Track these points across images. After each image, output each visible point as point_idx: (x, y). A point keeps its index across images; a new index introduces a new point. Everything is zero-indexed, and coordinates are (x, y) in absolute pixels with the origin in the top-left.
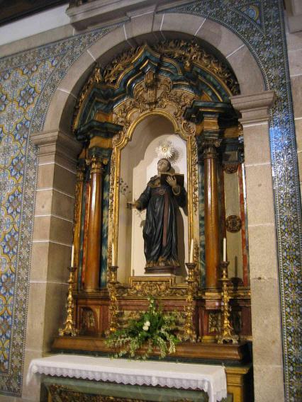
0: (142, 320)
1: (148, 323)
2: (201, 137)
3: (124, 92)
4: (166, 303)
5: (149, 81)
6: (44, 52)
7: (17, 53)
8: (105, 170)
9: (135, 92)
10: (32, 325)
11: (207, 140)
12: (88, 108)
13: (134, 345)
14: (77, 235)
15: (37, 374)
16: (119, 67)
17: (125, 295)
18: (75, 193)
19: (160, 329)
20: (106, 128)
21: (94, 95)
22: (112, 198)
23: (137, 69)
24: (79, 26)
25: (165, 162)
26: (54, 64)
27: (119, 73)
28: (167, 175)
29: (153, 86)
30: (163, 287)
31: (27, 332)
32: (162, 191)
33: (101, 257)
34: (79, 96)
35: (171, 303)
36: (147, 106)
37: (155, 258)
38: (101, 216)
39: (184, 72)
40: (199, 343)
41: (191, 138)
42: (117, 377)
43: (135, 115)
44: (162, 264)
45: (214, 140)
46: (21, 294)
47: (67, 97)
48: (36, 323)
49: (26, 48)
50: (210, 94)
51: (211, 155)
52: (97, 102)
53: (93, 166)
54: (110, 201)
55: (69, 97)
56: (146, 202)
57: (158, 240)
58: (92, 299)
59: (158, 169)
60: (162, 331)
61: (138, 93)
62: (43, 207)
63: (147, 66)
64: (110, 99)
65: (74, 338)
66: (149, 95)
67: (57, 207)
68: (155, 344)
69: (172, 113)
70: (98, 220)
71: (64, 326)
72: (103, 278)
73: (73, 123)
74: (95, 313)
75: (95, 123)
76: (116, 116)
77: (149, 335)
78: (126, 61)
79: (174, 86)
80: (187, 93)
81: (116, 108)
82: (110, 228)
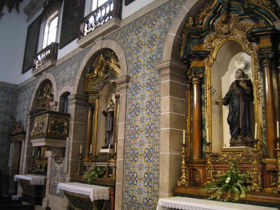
0: (226, 177)
1: (229, 179)
2: (260, 52)
3: (209, 29)
4: (243, 166)
5: (223, 19)
6: (159, 12)
7: (144, 15)
8: (201, 82)
9: (216, 28)
10: (163, 179)
11: (263, 54)
12: (188, 42)
13: (220, 192)
14: (188, 124)
15: (162, 206)
16: (204, 13)
17: (217, 160)
18: (185, 97)
19: (236, 182)
20: (199, 55)
21: (189, 35)
22: (206, 99)
23: (215, 13)
24: (83, 46)
25: (240, 71)
26: (165, 18)
27: (204, 17)
28: (239, 81)
29: (226, 22)
30: (240, 155)
31: (160, 183)
32: (238, 92)
33: (202, 136)
34: (182, 36)
35: (246, 166)
36: (224, 36)
37: (235, 136)
38: (200, 111)
39: (244, 9)
40: (262, 192)
41: (254, 53)
42: (183, 206)
43: (217, 43)
44: (240, 140)
45: (268, 54)
46: (156, 160)
47: (173, 39)
48: (165, 178)
49: (149, 11)
50: (263, 21)
51: (266, 65)
52: (192, 38)
53: (193, 80)
54: (206, 101)
55: (175, 38)
56: (228, 100)
57: (236, 124)
58: (197, 163)
59: (236, 77)
60: (238, 184)
61: (218, 28)
62: (165, 108)
63: (221, 9)
64: (201, 35)
65: (186, 187)
66: (224, 29)
67: (173, 107)
68: (233, 192)
69: (240, 38)
70: (199, 113)
71: (180, 180)
72: (204, 150)
73: (180, 54)
74: (198, 172)
75: (191, 53)
76: (205, 46)
77: (229, 186)
78: (209, 8)
79: (240, 20)
80: (249, 23)
81: (205, 41)
82: (206, 118)
